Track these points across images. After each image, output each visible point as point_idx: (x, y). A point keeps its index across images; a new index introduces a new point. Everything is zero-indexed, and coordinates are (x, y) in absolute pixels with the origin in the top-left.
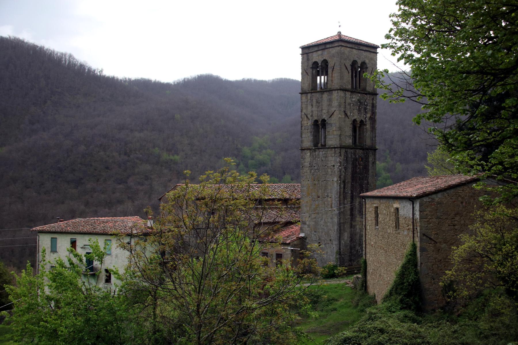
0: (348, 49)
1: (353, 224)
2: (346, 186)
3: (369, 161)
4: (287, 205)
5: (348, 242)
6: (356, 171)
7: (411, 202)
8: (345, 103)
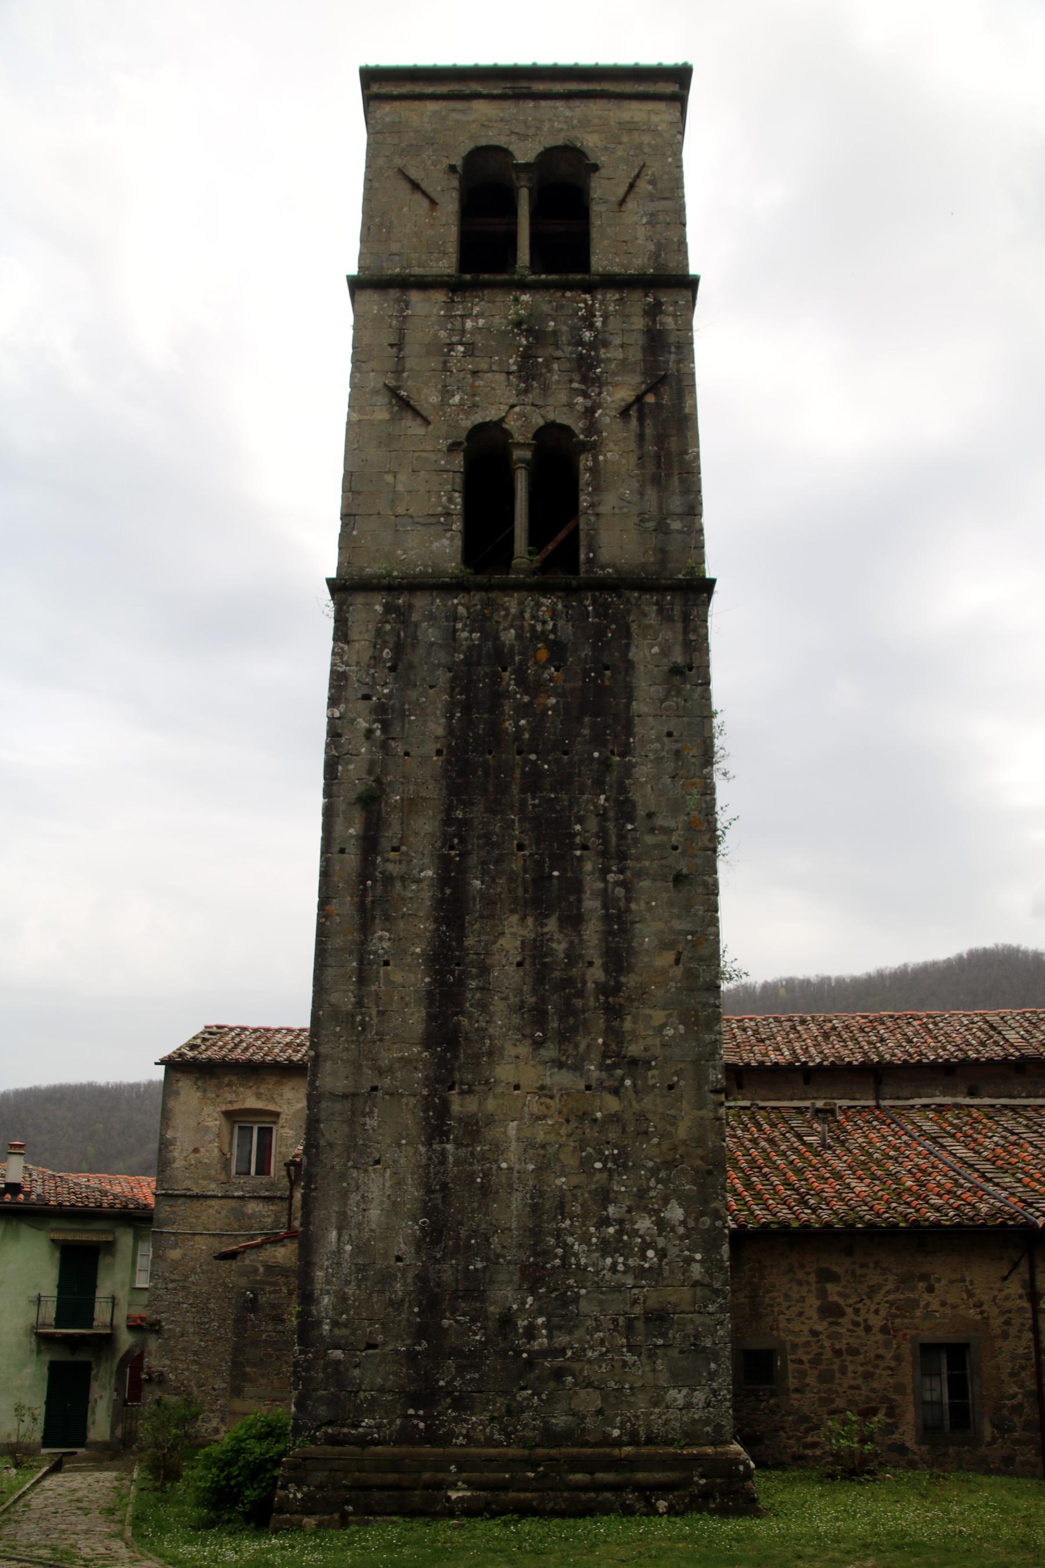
0: (432, 106)
2: (392, 833)
3: (630, 665)
4: (877, 1098)
5: (402, 1246)
6: (495, 731)
8: (398, 346)
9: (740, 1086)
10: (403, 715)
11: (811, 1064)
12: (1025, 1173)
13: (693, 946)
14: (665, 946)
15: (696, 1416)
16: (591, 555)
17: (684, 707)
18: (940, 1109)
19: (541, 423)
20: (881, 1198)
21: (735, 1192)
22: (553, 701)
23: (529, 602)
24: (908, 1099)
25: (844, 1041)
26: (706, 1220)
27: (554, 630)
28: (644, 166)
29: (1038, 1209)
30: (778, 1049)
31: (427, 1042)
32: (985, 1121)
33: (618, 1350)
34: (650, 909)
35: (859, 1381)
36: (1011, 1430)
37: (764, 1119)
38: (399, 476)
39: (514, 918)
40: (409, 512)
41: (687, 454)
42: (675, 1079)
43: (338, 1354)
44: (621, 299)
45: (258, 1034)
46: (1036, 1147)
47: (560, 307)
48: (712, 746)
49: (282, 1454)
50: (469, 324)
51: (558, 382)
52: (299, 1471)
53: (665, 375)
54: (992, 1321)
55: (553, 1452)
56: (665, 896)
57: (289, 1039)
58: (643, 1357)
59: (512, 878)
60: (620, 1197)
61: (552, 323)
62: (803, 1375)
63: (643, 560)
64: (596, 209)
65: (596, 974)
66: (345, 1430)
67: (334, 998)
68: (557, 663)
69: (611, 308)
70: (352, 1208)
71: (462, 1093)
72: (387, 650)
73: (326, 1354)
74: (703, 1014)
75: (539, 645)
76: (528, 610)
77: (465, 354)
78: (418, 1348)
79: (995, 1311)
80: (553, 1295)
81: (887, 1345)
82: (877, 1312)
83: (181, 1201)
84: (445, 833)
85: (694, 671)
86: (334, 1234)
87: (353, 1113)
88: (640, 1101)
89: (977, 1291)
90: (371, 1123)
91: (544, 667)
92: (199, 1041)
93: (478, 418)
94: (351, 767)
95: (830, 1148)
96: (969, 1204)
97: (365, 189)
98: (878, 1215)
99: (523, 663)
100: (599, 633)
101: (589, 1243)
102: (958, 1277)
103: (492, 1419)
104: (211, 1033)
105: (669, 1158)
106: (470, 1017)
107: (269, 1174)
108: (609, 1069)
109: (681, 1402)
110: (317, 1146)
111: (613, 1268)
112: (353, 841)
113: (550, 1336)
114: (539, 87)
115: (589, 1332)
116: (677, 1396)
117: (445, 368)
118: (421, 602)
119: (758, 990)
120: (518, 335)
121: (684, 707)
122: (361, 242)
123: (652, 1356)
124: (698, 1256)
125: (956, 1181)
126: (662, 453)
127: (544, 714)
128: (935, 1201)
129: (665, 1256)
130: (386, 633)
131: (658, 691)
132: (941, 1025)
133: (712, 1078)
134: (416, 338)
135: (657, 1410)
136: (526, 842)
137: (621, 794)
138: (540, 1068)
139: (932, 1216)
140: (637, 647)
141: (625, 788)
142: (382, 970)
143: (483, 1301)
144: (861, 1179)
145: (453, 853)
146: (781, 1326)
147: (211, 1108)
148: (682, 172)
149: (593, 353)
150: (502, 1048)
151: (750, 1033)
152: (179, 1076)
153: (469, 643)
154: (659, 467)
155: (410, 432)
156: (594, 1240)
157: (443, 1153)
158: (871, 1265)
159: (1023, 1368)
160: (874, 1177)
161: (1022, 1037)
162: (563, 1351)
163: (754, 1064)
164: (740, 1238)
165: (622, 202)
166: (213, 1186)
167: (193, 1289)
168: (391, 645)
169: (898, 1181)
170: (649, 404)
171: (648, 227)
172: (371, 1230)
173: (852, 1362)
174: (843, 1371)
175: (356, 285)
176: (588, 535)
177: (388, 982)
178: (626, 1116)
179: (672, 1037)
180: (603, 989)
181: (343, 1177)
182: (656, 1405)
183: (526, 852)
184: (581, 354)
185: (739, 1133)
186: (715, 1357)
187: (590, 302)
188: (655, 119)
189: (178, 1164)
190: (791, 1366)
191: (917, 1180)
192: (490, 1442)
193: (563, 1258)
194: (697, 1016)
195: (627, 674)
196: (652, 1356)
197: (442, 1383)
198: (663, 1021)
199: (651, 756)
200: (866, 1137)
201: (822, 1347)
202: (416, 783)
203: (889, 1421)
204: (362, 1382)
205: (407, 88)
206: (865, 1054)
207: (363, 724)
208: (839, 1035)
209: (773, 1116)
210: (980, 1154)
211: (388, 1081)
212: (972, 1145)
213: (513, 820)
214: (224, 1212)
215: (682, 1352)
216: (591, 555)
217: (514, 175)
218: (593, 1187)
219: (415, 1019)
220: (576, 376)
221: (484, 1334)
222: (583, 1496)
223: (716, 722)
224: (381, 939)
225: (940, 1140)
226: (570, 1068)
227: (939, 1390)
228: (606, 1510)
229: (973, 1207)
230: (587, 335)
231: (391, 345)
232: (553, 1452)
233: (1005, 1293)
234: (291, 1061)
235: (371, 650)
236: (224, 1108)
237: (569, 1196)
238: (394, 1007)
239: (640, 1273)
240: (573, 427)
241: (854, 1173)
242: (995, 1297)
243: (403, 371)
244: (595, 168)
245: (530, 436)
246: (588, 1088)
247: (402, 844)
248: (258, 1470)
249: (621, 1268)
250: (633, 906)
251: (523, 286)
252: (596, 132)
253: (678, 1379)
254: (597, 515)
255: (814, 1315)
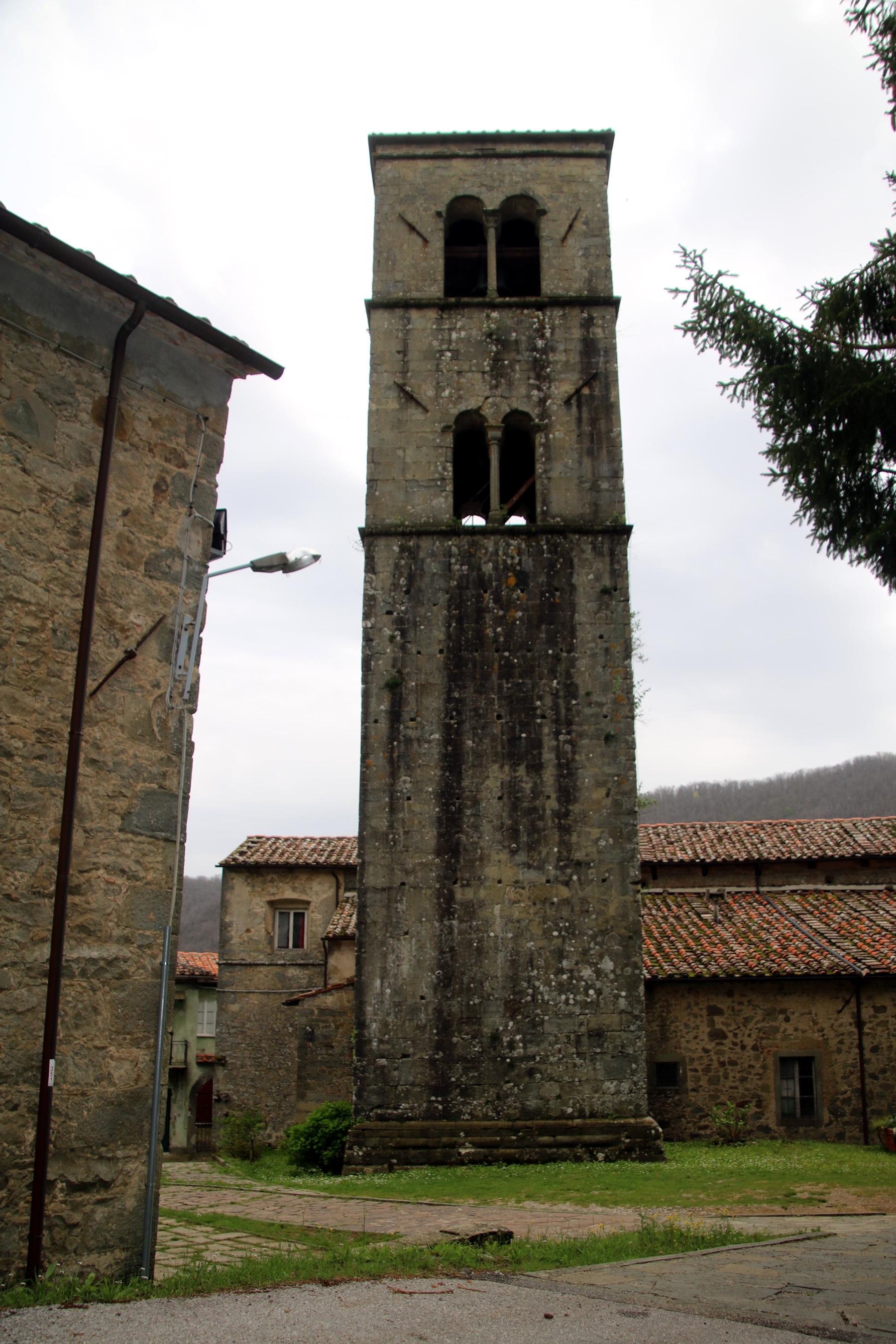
0: (422, 164)
1: (461, 894)
2: (409, 709)
3: (573, 588)
4: (758, 885)
6: (480, 635)
7: (334, 880)
8: (404, 352)
9: (655, 878)
10: (415, 625)
11: (708, 861)
12: (861, 940)
13: (619, 784)
14: (599, 784)
15: (623, 1099)
16: (545, 508)
17: (611, 618)
18: (804, 893)
19: (508, 410)
20: (754, 957)
21: (650, 954)
22: (520, 614)
23: (502, 543)
24: (780, 886)
25: (734, 843)
26: (629, 970)
27: (520, 563)
28: (580, 210)
29: (864, 964)
30: (683, 849)
31: (438, 853)
32: (836, 902)
33: (570, 1056)
34: (588, 759)
35: (737, 1083)
36: (843, 1115)
37: (673, 901)
38: (407, 451)
39: (496, 767)
40: (416, 478)
41: (612, 432)
42: (607, 875)
43: (383, 1061)
44: (564, 315)
45: (289, 842)
46: (871, 921)
47: (520, 322)
48: (630, 639)
49: (349, 1127)
50: (454, 335)
51: (519, 379)
52: (360, 1138)
53: (596, 373)
54: (830, 1041)
55: (529, 1123)
56: (599, 750)
57: (313, 845)
58: (587, 1061)
59: (494, 739)
60: (570, 954)
61: (514, 334)
62: (698, 1079)
63: (582, 511)
64: (545, 244)
65: (552, 804)
66: (389, 1111)
67: (374, 822)
68: (522, 587)
69: (557, 322)
70: (390, 964)
71: (463, 886)
72: (403, 579)
73: (375, 1062)
74: (625, 831)
75: (510, 574)
76: (501, 549)
77: (452, 359)
78: (436, 1056)
79: (832, 1034)
80: (527, 1020)
81: (757, 1058)
82: (749, 1036)
83: (238, 968)
84: (446, 709)
85: (618, 592)
86: (378, 982)
87: (389, 900)
88: (583, 890)
89: (820, 1021)
90: (401, 907)
91: (513, 590)
92: (245, 849)
93: (462, 407)
94: (380, 662)
95: (720, 922)
96: (816, 961)
97: (375, 230)
98: (751, 968)
99: (498, 588)
100: (552, 565)
101: (550, 986)
102: (807, 1011)
103: (487, 1102)
104: (253, 842)
105: (603, 928)
106: (467, 835)
107: (302, 947)
108: (562, 869)
109: (613, 1090)
110: (365, 923)
111: (567, 1002)
112: (383, 714)
113: (525, 1048)
114: (501, 148)
115: (550, 1044)
116: (611, 1086)
117: (438, 370)
118: (426, 544)
119: (675, 793)
120: (490, 343)
121: (611, 618)
122: (374, 272)
123: (593, 1060)
124: (623, 994)
125: (810, 945)
126: (595, 432)
127: (514, 623)
128: (792, 958)
129: (601, 994)
130: (402, 566)
131: (592, 606)
132: (807, 830)
133: (632, 874)
134: (417, 347)
135: (597, 1095)
136: (503, 714)
137: (567, 679)
138: (516, 868)
139: (788, 968)
140: (578, 574)
141: (571, 675)
142: (406, 803)
143: (480, 1025)
144: (741, 944)
145: (452, 722)
146: (682, 1046)
147: (259, 899)
148: (607, 215)
149: (544, 357)
150: (489, 855)
151: (662, 837)
152: (233, 875)
153: (460, 573)
154: (592, 441)
155: (414, 418)
156: (553, 983)
157: (451, 927)
158: (746, 1003)
159: (851, 1073)
160: (751, 943)
161: (868, 839)
162: (534, 1058)
163: (665, 861)
164: (652, 985)
165: (564, 239)
166: (261, 957)
167: (249, 1033)
168: (406, 575)
169: (768, 945)
170: (585, 395)
171: (583, 259)
172: (403, 979)
173: (732, 1070)
174: (726, 1077)
175: (371, 306)
176: (542, 493)
177: (411, 811)
178: (574, 900)
179: (605, 847)
180: (557, 815)
181: (383, 943)
182: (596, 1092)
183: (503, 721)
184: (535, 357)
185: (654, 912)
186: (636, 1061)
187: (541, 318)
188: (587, 173)
189: (235, 941)
190: (689, 1074)
191: (782, 945)
192: (486, 1117)
193: (533, 996)
194: (621, 832)
195: (571, 594)
196: (593, 1060)
197: (453, 1079)
198: (598, 835)
199: (589, 652)
200: (747, 914)
201: (711, 1060)
202: (426, 674)
203: (758, 1110)
204: (400, 1079)
205: (404, 150)
206: (749, 852)
207: (387, 632)
208: (730, 839)
209: (679, 899)
210: (829, 926)
211: (412, 878)
212: (825, 920)
213: (494, 699)
214: (270, 976)
215: (613, 1057)
216: (545, 508)
217: (484, 218)
218: (552, 948)
219: (429, 836)
220: (532, 375)
221: (480, 1047)
222: (549, 1151)
223: (633, 621)
224: (405, 782)
225: (802, 916)
226: (535, 868)
227: (793, 1089)
228: (563, 1158)
229: (819, 962)
230: (540, 343)
231: (399, 352)
232: (529, 1123)
233: (839, 1022)
234: (318, 863)
235: (392, 579)
236: (268, 898)
237: (536, 955)
238: (415, 828)
239: (585, 1005)
240: (531, 413)
241: (736, 940)
242: (832, 1025)
243: (407, 372)
244: (544, 212)
245: (500, 420)
246: (548, 881)
247: (418, 716)
248: (331, 1138)
249: (571, 1002)
250: (577, 757)
251: (493, 306)
252: (544, 183)
253: (612, 1074)
254: (549, 478)
255: (706, 1038)
